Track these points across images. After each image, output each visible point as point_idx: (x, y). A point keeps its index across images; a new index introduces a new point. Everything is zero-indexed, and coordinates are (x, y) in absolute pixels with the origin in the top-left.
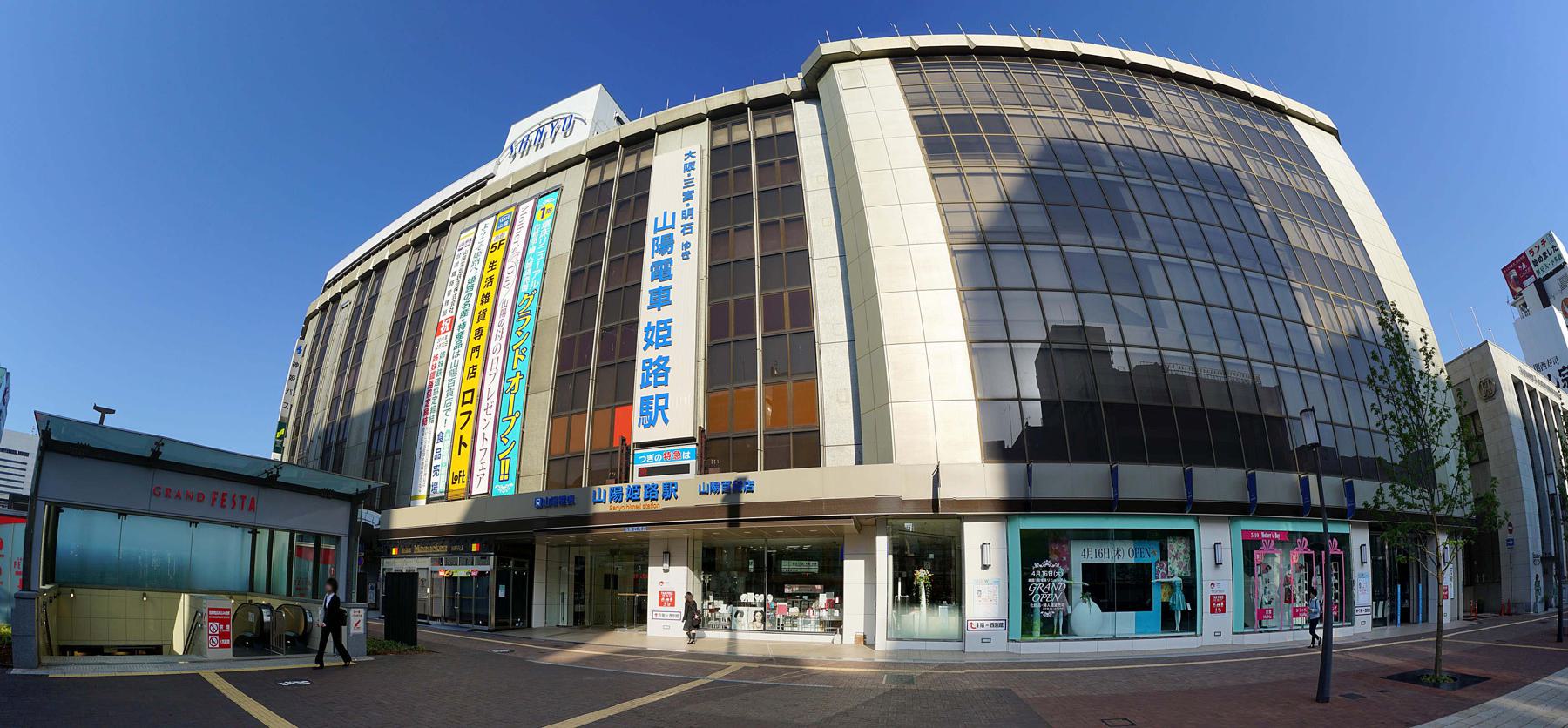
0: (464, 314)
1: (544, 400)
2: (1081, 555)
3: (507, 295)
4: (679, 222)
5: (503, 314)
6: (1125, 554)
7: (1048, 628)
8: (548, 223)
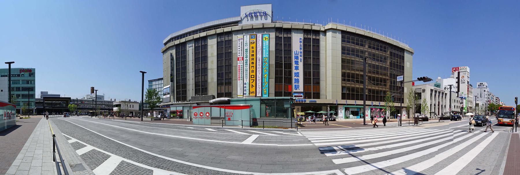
0: (246, 57)
1: (273, 81)
2: (351, 110)
3: (259, 56)
4: (299, 54)
5: (259, 60)
6: (356, 110)
7: (347, 118)
8: (268, 42)
